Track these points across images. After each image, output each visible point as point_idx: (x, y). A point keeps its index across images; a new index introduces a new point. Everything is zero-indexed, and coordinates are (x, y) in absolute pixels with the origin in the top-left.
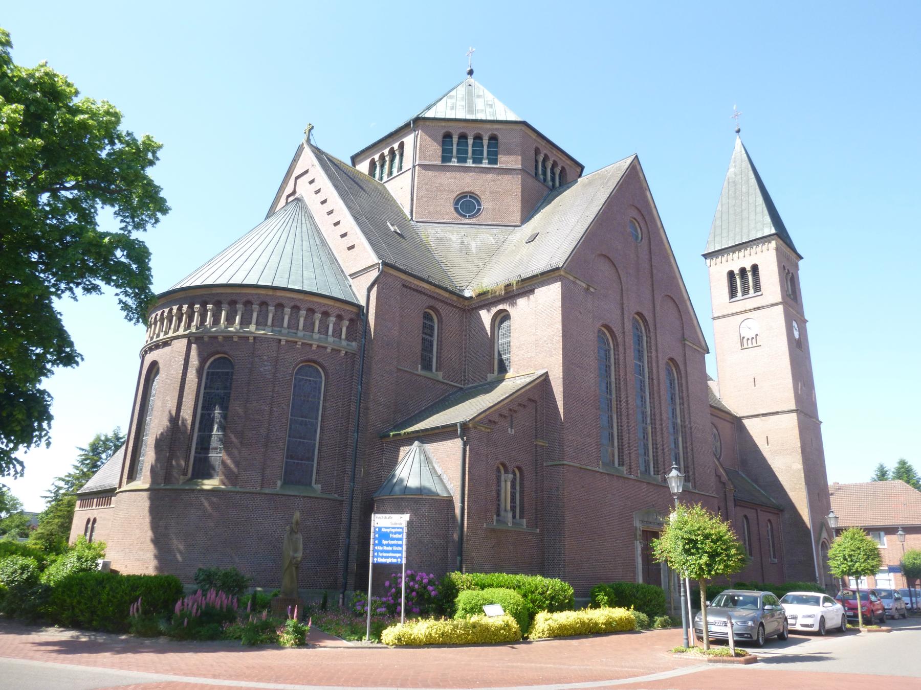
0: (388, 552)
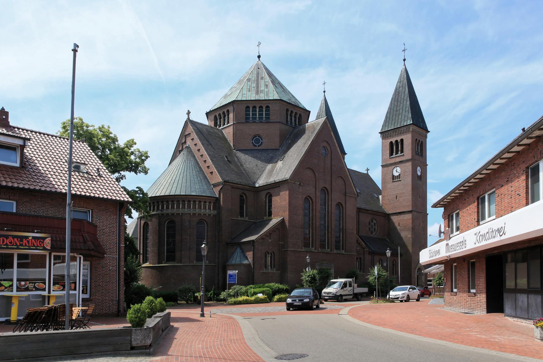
0: (232, 280)
